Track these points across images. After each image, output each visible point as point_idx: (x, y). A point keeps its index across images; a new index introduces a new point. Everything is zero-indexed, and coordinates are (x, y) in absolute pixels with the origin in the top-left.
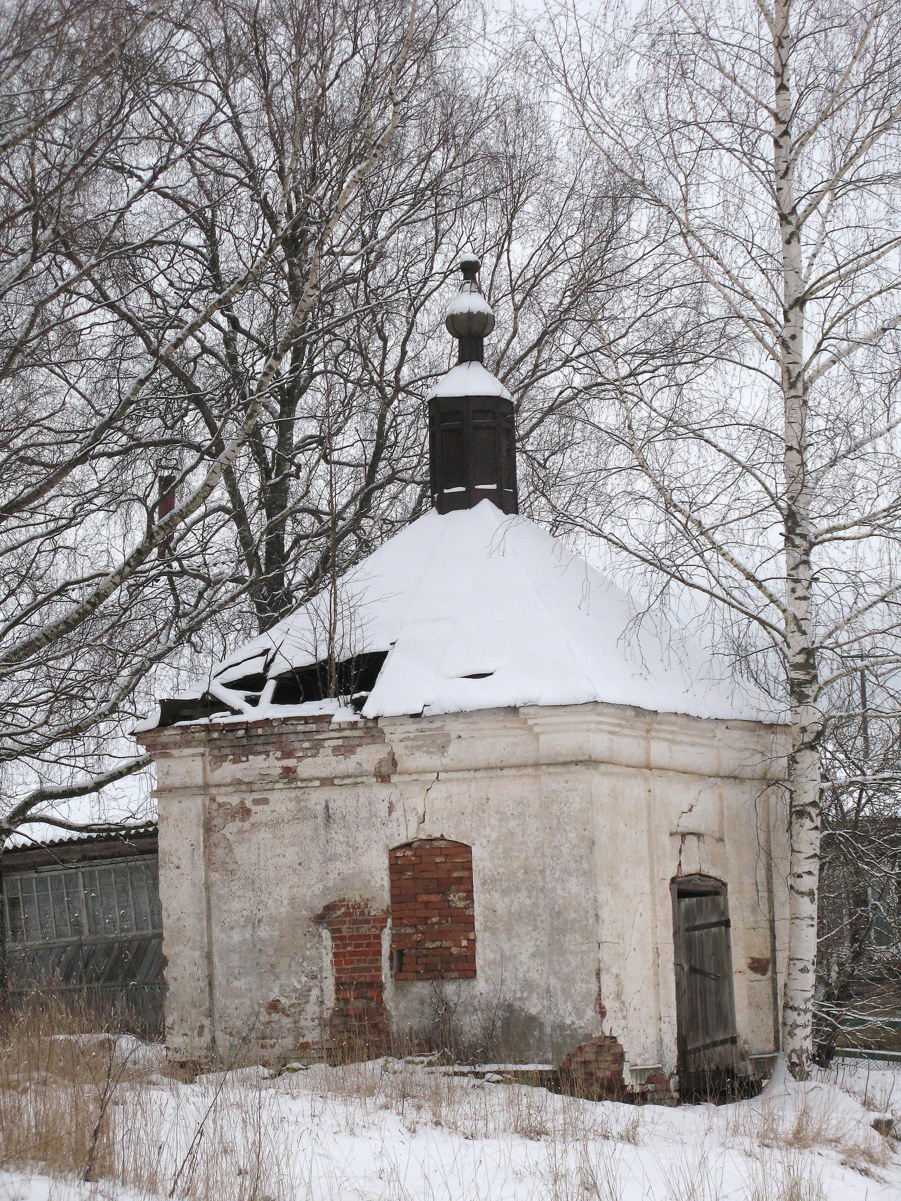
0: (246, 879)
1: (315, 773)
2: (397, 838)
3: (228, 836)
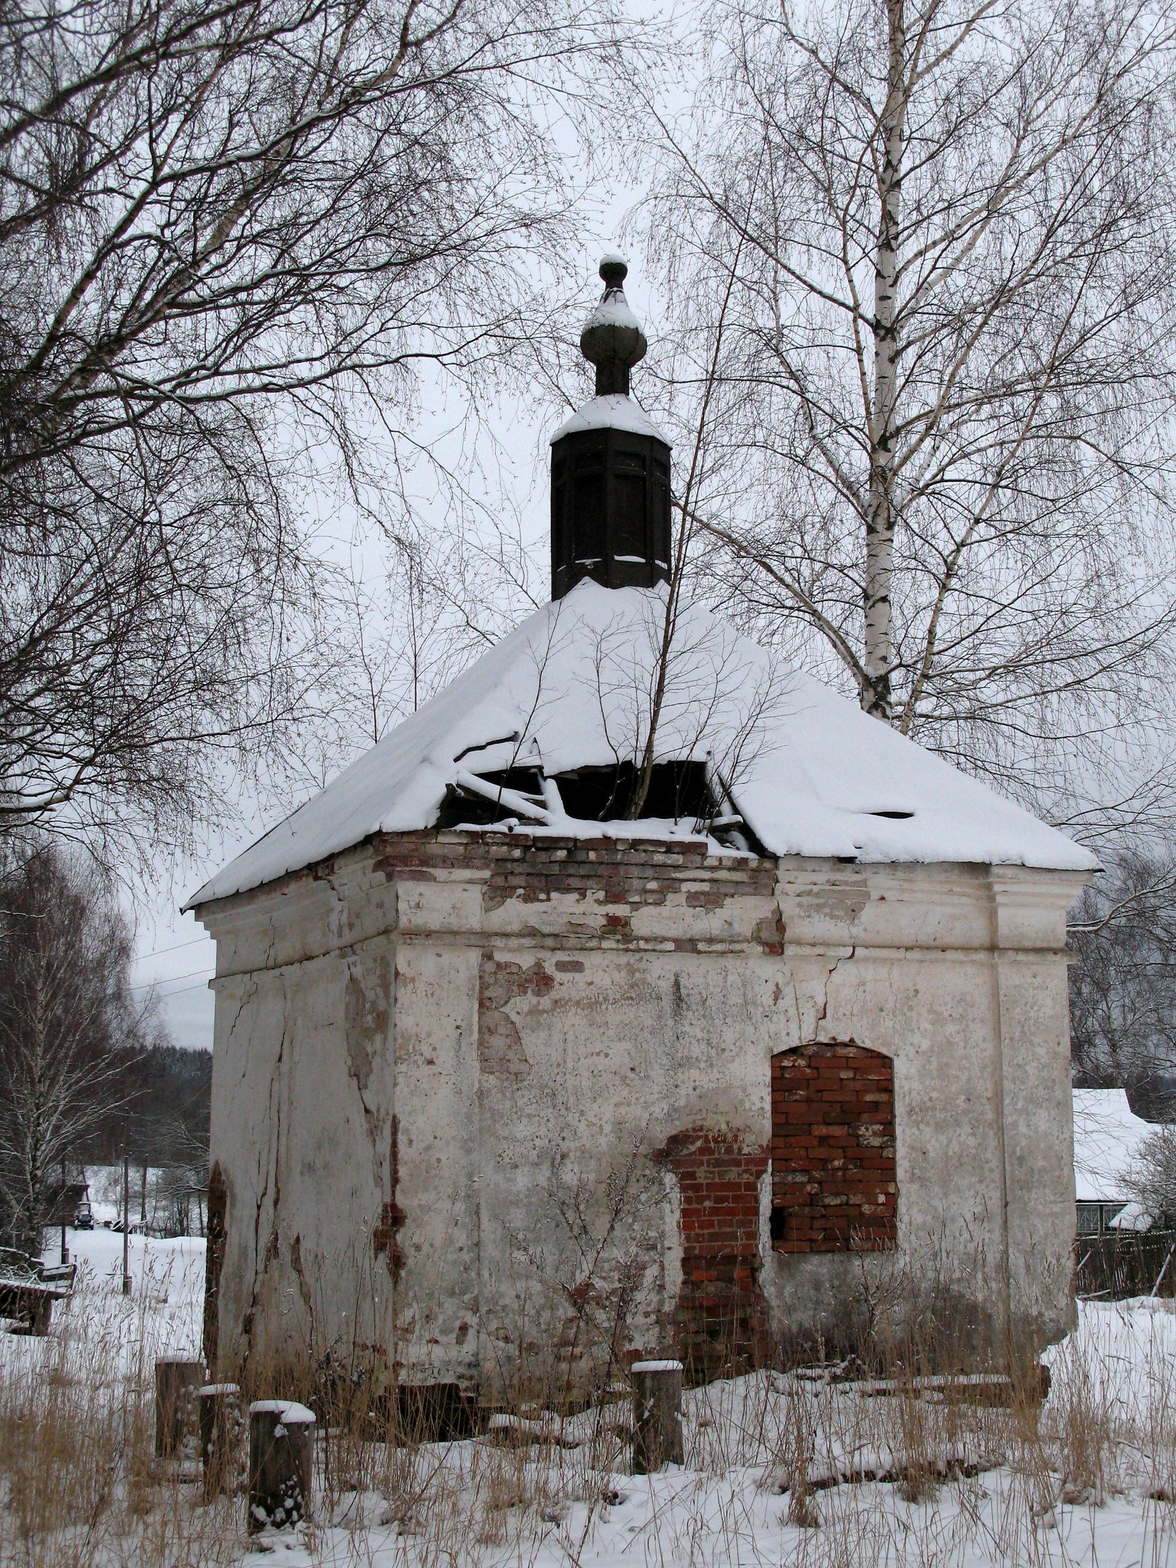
0: (542, 1087)
1: (658, 930)
2: (785, 1038)
3: (514, 1017)
